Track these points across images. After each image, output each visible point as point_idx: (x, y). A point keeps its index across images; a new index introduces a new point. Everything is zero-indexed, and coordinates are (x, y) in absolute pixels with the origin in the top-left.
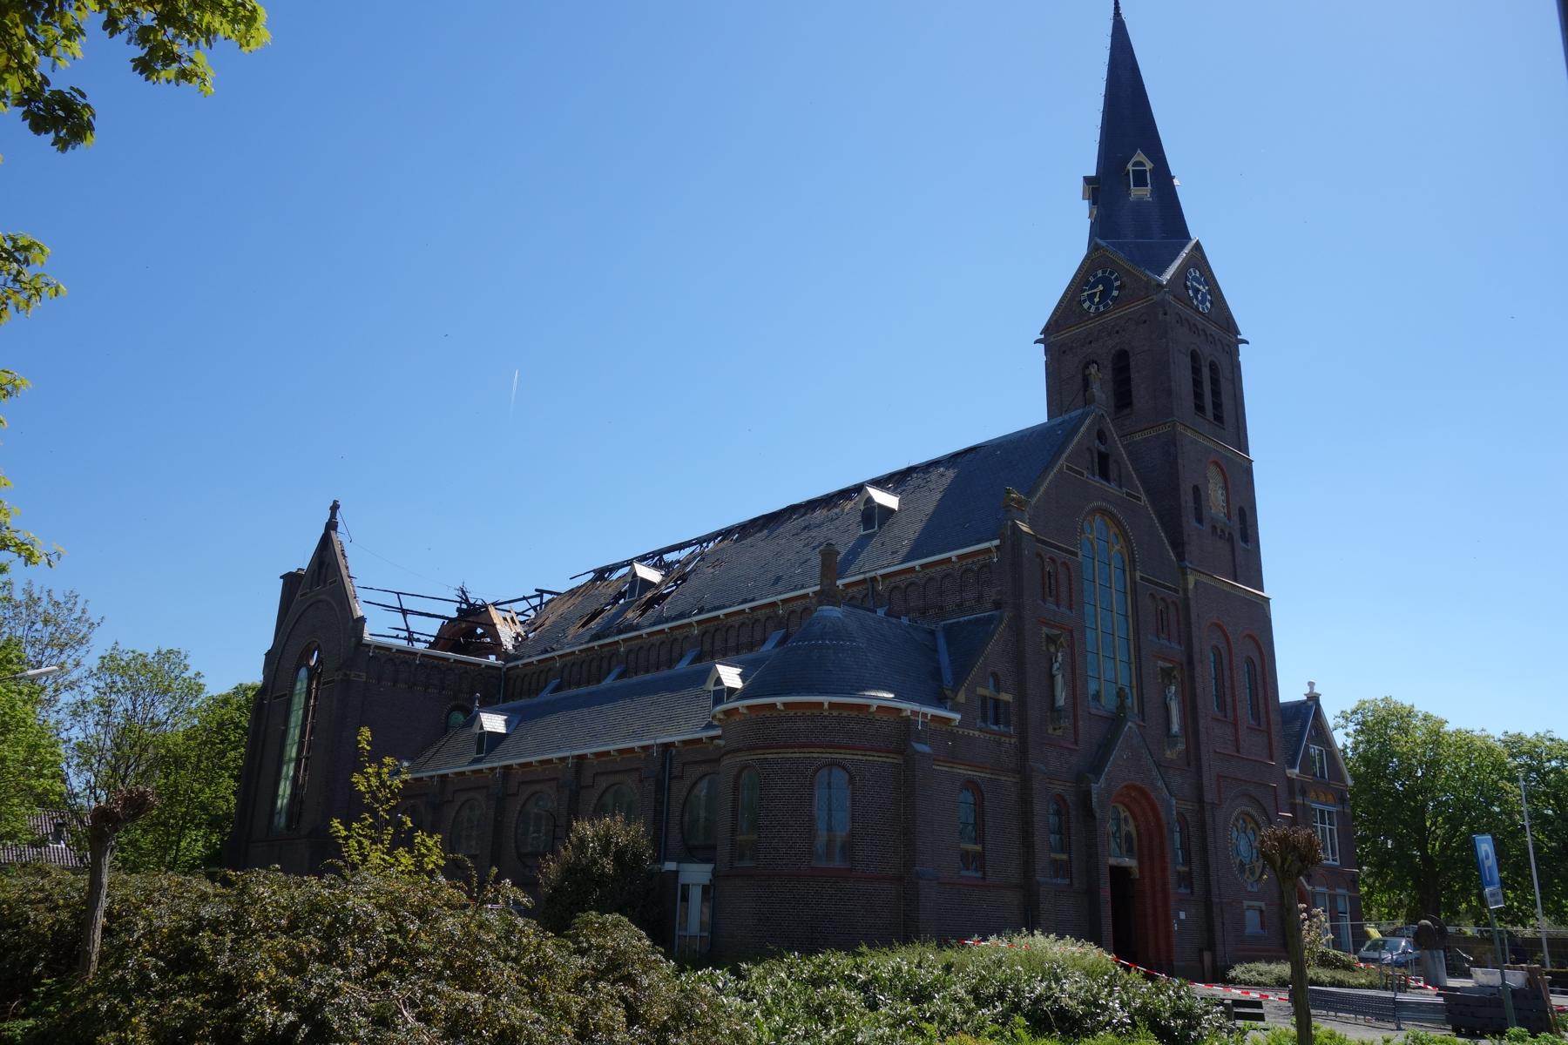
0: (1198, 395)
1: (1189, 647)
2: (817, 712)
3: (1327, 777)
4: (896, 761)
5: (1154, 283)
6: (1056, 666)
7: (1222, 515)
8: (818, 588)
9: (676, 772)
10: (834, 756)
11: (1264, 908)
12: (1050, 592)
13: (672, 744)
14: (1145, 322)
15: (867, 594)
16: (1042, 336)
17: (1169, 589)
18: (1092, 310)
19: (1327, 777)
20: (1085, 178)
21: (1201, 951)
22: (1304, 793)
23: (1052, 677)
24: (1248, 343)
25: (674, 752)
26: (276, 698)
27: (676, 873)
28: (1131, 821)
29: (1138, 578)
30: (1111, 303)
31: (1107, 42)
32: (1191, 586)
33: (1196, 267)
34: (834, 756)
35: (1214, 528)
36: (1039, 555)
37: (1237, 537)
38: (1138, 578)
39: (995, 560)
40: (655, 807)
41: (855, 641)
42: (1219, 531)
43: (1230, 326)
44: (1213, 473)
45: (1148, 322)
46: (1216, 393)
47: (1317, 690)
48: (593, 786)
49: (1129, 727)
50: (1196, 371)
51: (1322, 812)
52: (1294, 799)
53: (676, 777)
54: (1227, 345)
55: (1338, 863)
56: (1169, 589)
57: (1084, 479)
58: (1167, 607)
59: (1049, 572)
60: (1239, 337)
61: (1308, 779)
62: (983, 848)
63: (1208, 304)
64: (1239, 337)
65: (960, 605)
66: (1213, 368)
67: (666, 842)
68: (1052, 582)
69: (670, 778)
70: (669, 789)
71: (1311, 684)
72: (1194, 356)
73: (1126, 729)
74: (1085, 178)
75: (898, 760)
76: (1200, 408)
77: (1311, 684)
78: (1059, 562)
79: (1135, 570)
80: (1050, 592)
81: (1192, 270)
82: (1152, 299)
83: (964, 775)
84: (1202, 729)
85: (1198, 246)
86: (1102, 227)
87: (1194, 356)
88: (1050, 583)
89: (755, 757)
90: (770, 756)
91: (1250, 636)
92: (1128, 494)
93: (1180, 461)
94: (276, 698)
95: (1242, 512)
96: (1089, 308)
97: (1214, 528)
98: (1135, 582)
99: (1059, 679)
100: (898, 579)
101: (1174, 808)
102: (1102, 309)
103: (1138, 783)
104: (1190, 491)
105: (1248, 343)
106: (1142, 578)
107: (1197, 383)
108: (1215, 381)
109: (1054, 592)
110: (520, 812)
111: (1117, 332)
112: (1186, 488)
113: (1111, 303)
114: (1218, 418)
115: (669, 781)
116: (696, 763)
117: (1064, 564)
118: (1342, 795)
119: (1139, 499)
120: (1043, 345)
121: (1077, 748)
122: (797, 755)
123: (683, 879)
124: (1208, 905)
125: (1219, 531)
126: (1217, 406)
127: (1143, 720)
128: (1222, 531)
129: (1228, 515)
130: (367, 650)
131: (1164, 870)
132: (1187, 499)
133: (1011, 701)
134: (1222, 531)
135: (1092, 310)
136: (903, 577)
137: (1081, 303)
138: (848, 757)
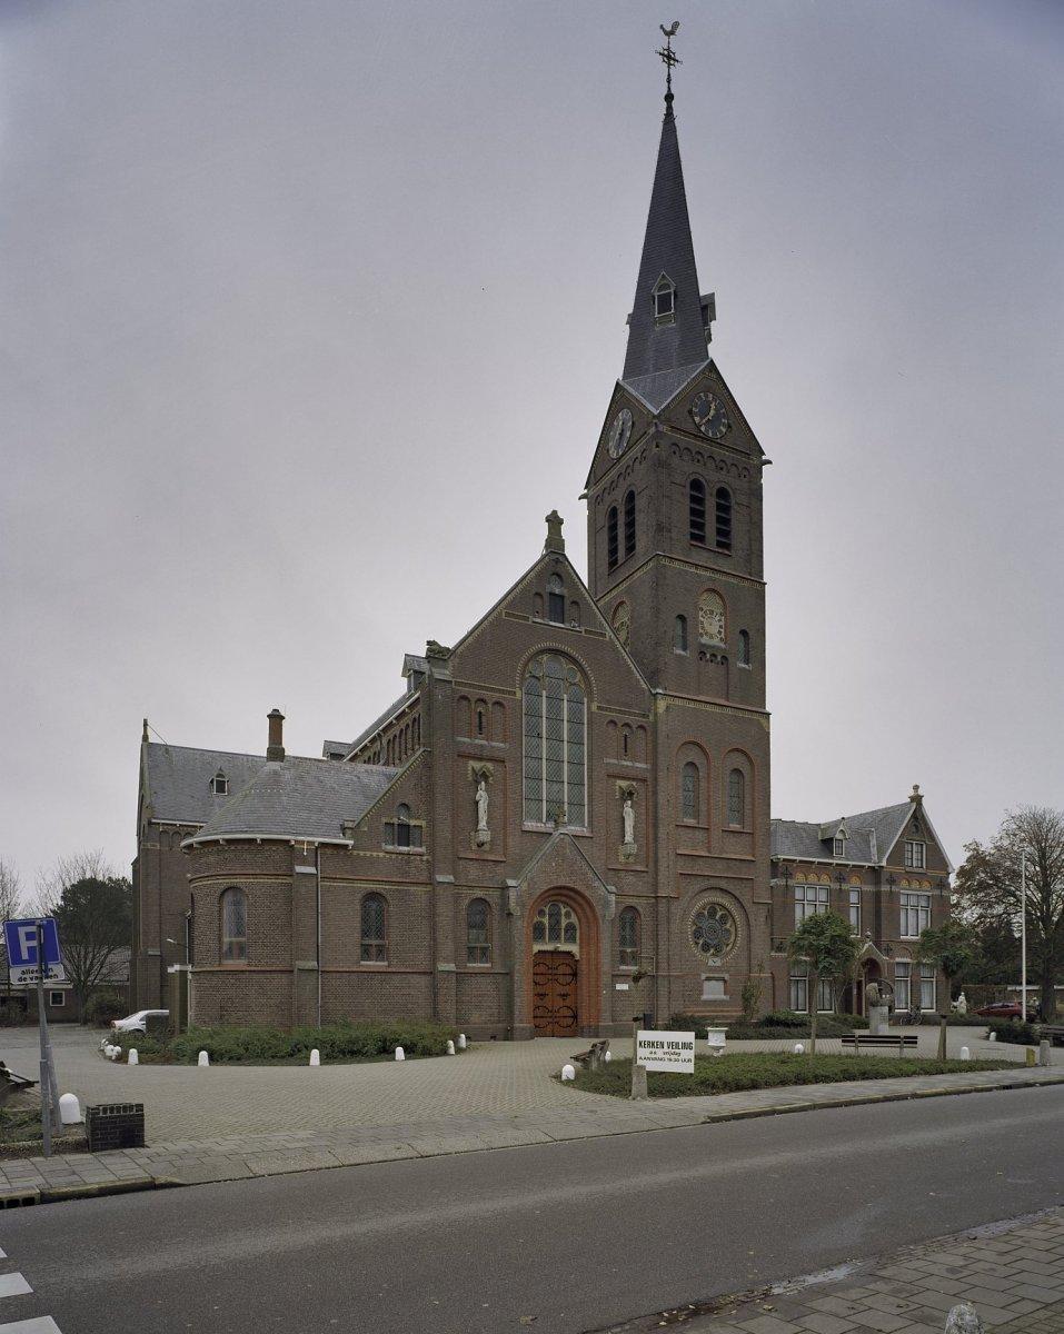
22: (892, 881)
47: (920, 792)
59: (480, 713)
61: (898, 869)
71: (916, 788)
72: (696, 485)
77: (916, 788)
87: (696, 485)
103: (563, 882)
134: (714, 655)
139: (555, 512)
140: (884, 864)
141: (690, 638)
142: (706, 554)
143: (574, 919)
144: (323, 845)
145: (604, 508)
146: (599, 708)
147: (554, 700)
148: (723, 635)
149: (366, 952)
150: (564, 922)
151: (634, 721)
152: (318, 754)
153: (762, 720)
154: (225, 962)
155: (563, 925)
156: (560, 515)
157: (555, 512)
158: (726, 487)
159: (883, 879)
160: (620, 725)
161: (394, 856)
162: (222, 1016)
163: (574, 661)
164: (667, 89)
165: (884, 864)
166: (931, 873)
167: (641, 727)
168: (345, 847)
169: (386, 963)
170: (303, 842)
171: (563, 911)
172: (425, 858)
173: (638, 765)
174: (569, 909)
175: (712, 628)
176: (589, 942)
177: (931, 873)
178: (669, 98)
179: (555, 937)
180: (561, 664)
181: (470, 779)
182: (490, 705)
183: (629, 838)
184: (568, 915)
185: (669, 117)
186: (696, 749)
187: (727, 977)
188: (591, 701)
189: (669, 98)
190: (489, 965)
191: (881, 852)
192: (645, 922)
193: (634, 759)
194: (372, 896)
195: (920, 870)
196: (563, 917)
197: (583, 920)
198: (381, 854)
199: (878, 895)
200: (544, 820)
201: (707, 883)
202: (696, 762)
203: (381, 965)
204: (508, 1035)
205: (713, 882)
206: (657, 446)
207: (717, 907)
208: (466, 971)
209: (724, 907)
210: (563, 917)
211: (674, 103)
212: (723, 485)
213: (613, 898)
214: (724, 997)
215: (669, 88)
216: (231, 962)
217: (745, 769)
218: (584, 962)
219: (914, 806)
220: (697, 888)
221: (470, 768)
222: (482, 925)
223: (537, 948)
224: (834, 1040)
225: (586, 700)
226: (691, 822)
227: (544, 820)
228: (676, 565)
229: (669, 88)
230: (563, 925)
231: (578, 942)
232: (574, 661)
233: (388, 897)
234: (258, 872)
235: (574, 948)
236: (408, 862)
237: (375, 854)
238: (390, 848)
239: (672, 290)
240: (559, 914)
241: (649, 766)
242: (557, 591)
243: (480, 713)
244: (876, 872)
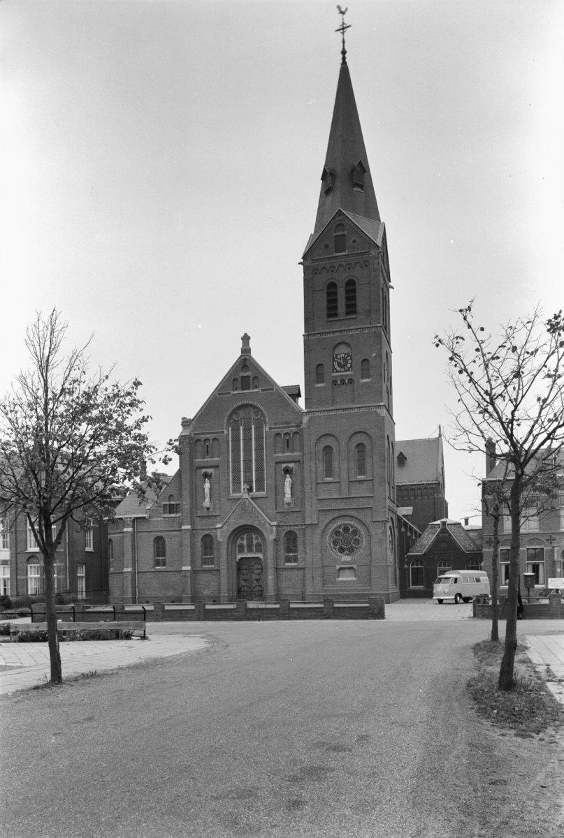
47: (140, 394)
139: (246, 334)
147: (248, 430)
149: (157, 563)
150: (255, 542)
152: (389, 610)
156: (249, 334)
157: (246, 334)
164: (342, 48)
168: (144, 518)
170: (127, 518)
171: (254, 537)
173: (295, 454)
178: (344, 52)
179: (250, 550)
184: (257, 539)
185: (344, 63)
187: (355, 566)
189: (344, 52)
190: (213, 566)
193: (292, 451)
201: (337, 514)
211: (346, 55)
215: (344, 46)
217: (366, 443)
220: (331, 518)
222: (241, 566)
223: (239, 557)
224: (499, 625)
226: (360, 477)
229: (344, 46)
235: (260, 555)
238: (166, 515)
240: (252, 538)
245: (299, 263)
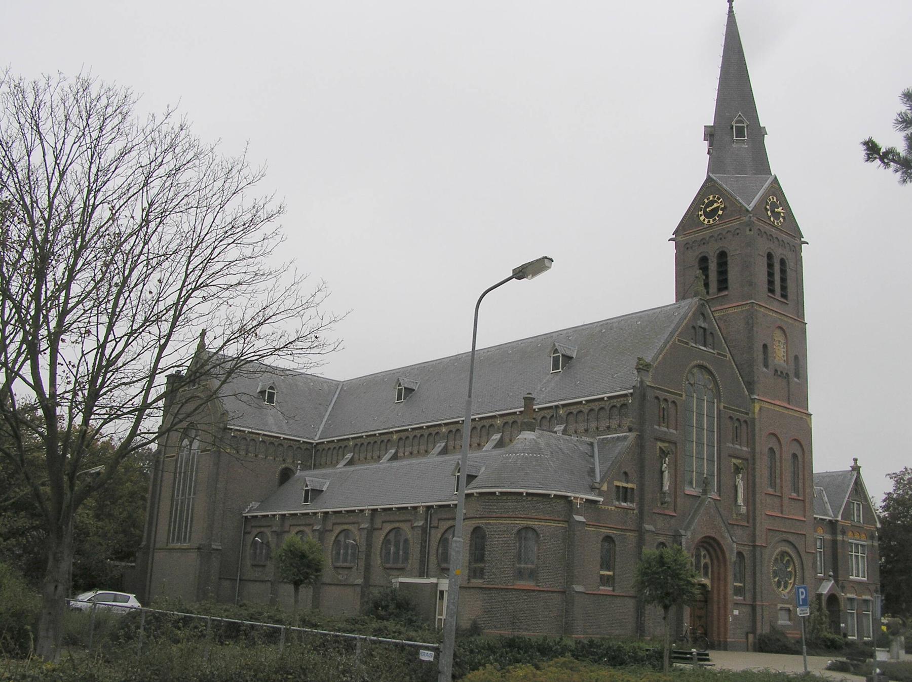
0: (771, 283)
1: (753, 449)
2: (519, 498)
3: (862, 522)
4: (563, 525)
5: (743, 209)
6: (665, 465)
7: (782, 361)
8: (523, 409)
9: (435, 524)
10: (528, 523)
11: (791, 609)
12: (663, 420)
13: (432, 507)
14: (738, 234)
15: (553, 416)
16: (674, 236)
17: (742, 412)
18: (706, 222)
19: (862, 522)
20: (705, 126)
21: (747, 634)
22: (844, 533)
23: (662, 472)
24: (808, 243)
25: (433, 511)
26: (168, 457)
27: (437, 584)
28: (707, 556)
29: (722, 408)
30: (717, 219)
31: (724, 30)
32: (757, 410)
33: (774, 194)
34: (528, 523)
35: (776, 371)
36: (657, 398)
37: (791, 375)
38: (722, 408)
39: (630, 401)
40: (421, 543)
41: (543, 454)
42: (779, 372)
43: (796, 233)
44: (778, 336)
45: (740, 234)
46: (783, 280)
47: (859, 464)
48: (381, 529)
49: (709, 502)
50: (770, 266)
51: (857, 545)
52: (836, 536)
53: (434, 527)
54: (793, 246)
55: (866, 579)
56: (742, 412)
57: (689, 347)
58: (741, 425)
59: (663, 408)
60: (802, 239)
61: (848, 523)
62: (614, 574)
63: (781, 219)
64: (802, 239)
65: (608, 427)
66: (783, 262)
67: (428, 566)
68: (665, 413)
69: (430, 527)
70: (430, 533)
71: (855, 460)
72: (770, 256)
73: (706, 503)
74: (705, 126)
75: (565, 525)
76: (771, 291)
77: (855, 460)
78: (670, 401)
79: (720, 402)
80: (663, 420)
81: (771, 197)
82: (742, 220)
83: (604, 533)
84: (758, 500)
85: (776, 180)
86: (716, 163)
87: (770, 256)
88: (664, 415)
89: (483, 522)
90: (492, 522)
91: (795, 440)
92: (719, 354)
93: (755, 329)
94: (168, 457)
95: (796, 357)
96: (704, 220)
97: (776, 371)
98: (720, 411)
99: (666, 474)
100: (572, 408)
101: (735, 549)
102: (711, 222)
103: (713, 535)
104: (761, 348)
105: (808, 243)
106: (725, 407)
107: (771, 275)
108: (783, 271)
109: (666, 420)
110: (335, 541)
111: (721, 239)
112: (759, 347)
113: (717, 219)
114: (784, 296)
115: (430, 530)
116: (445, 519)
117: (674, 402)
118: (872, 535)
119: (726, 356)
120: (674, 242)
121: (675, 515)
122: (508, 522)
123: (440, 588)
124: (754, 608)
125: (779, 372)
126: (784, 288)
127: (720, 496)
128: (782, 372)
129: (787, 361)
130: (230, 431)
131: (726, 586)
132: (759, 355)
133: (635, 488)
134: (782, 372)
135: (706, 222)
136: (575, 407)
137: (698, 216)
138: (536, 523)
140: (839, 518)
141: (770, 361)
142: (776, 303)
143: (708, 560)
144: (527, 528)
145: (693, 257)
146: (725, 407)
148: (785, 359)
150: (703, 561)
151: (743, 417)
153: (808, 419)
154: (473, 581)
155: (702, 564)
158: (785, 258)
159: (838, 531)
160: (735, 419)
161: (619, 510)
162: (513, 623)
163: (711, 373)
165: (839, 518)
166: (867, 527)
167: (745, 422)
169: (611, 589)
172: (635, 512)
174: (705, 552)
175: (779, 354)
176: (719, 578)
177: (867, 527)
180: (703, 375)
181: (658, 455)
182: (670, 403)
183: (740, 501)
186: (774, 439)
188: (719, 401)
191: (836, 512)
192: (748, 561)
194: (608, 539)
195: (858, 524)
196: (702, 558)
197: (715, 562)
198: (613, 508)
199: (834, 542)
200: (694, 486)
202: (774, 447)
203: (530, 584)
204: (748, 650)
205: (785, 536)
206: (750, 230)
207: (785, 554)
208: (599, 592)
209: (790, 557)
210: (702, 558)
212: (783, 256)
213: (735, 545)
214: (789, 622)
216: (522, 582)
218: (715, 592)
219: (855, 473)
221: (658, 447)
225: (716, 400)
227: (694, 486)
228: (762, 310)
230: (702, 564)
231: (710, 576)
232: (711, 373)
233: (616, 541)
234: (547, 518)
236: (627, 514)
237: (610, 507)
239: (745, 125)
241: (749, 450)
242: (703, 326)
243: (663, 408)
244: (833, 524)
245: (669, 240)
